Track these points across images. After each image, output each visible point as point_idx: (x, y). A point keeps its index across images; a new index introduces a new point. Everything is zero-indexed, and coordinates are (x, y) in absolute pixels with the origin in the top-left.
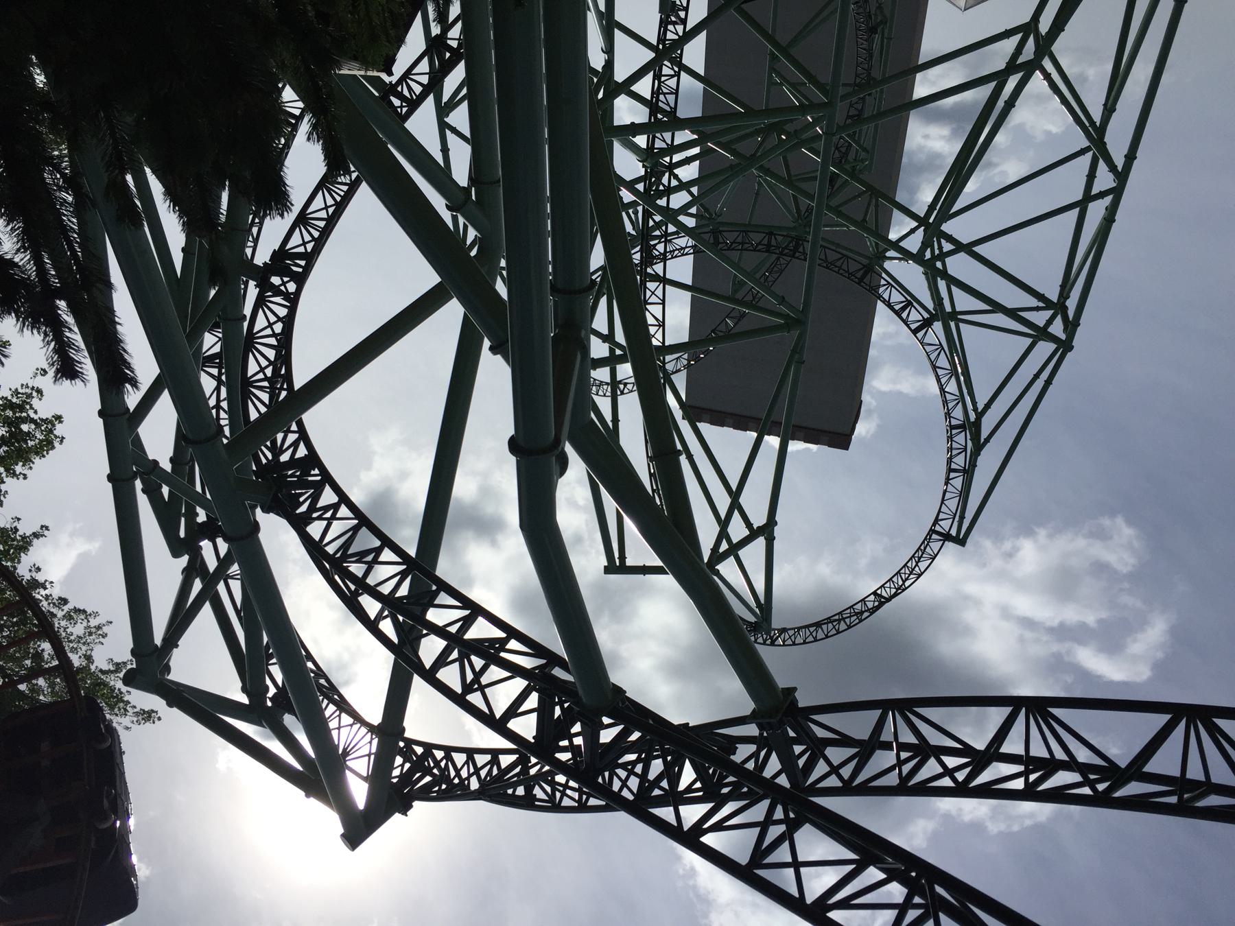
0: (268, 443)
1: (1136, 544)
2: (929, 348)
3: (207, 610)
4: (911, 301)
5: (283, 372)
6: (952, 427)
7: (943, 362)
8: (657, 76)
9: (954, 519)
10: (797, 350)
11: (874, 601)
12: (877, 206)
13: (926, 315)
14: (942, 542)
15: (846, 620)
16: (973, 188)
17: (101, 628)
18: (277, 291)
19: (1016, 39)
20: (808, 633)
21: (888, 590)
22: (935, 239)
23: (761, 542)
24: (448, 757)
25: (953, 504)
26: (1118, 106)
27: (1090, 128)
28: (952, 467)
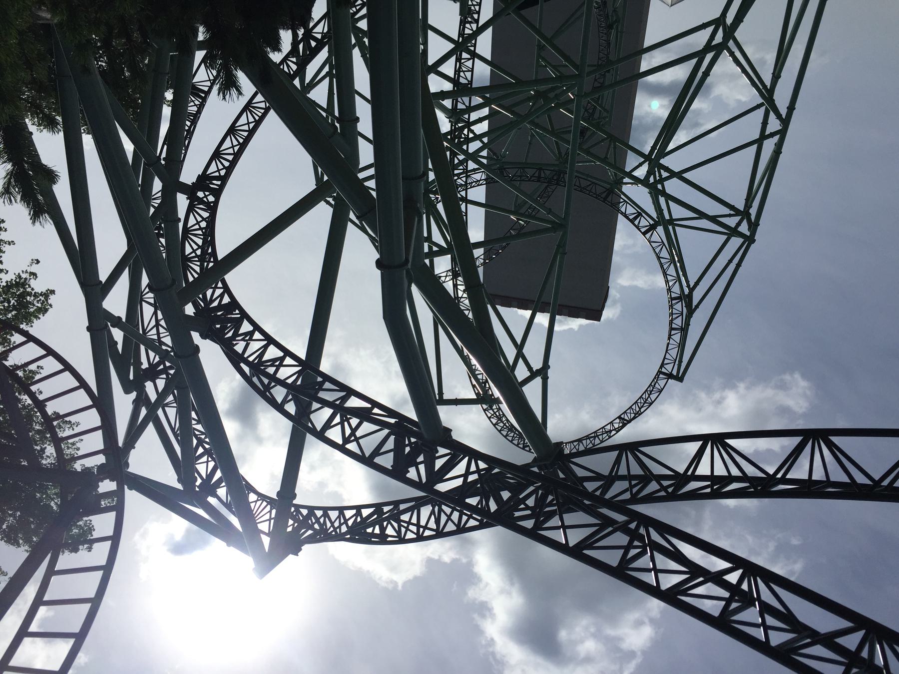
0: (201, 296)
1: (808, 393)
2: (654, 245)
3: (151, 428)
4: (641, 212)
5: (210, 251)
6: (672, 299)
7: (665, 254)
8: (459, 60)
9: (675, 363)
10: (561, 245)
11: (619, 423)
12: (615, 148)
13: (652, 222)
14: (667, 380)
15: (599, 437)
16: (681, 137)
17: (75, 444)
18: (201, 201)
19: (710, 29)
20: (573, 447)
21: (629, 415)
22: (656, 169)
23: (538, 381)
24: (325, 515)
25: (674, 353)
26: (782, 74)
27: (763, 90)
28: (673, 327)
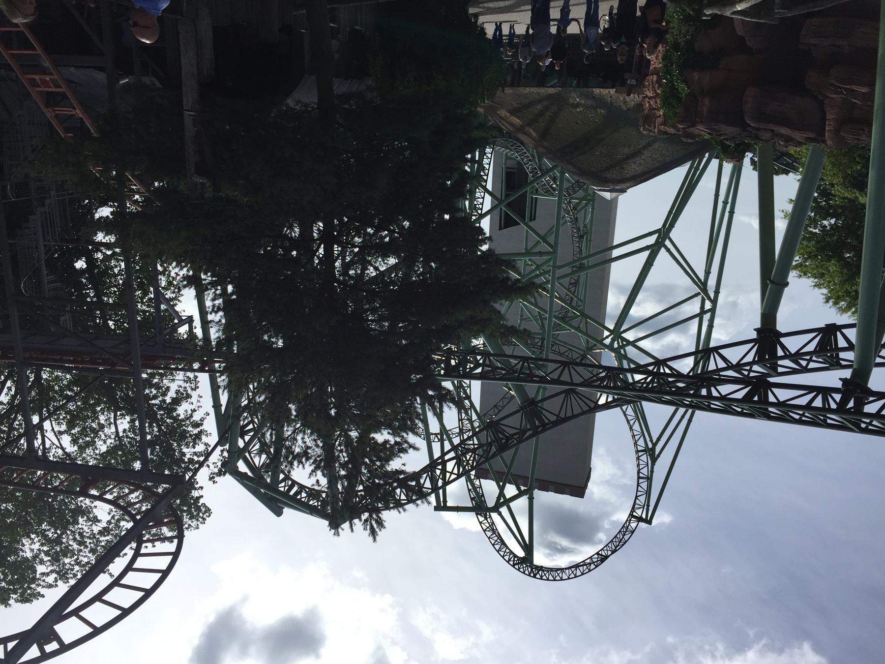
11: (598, 558)
20: (571, 572)
21: (606, 552)
25: (642, 499)
